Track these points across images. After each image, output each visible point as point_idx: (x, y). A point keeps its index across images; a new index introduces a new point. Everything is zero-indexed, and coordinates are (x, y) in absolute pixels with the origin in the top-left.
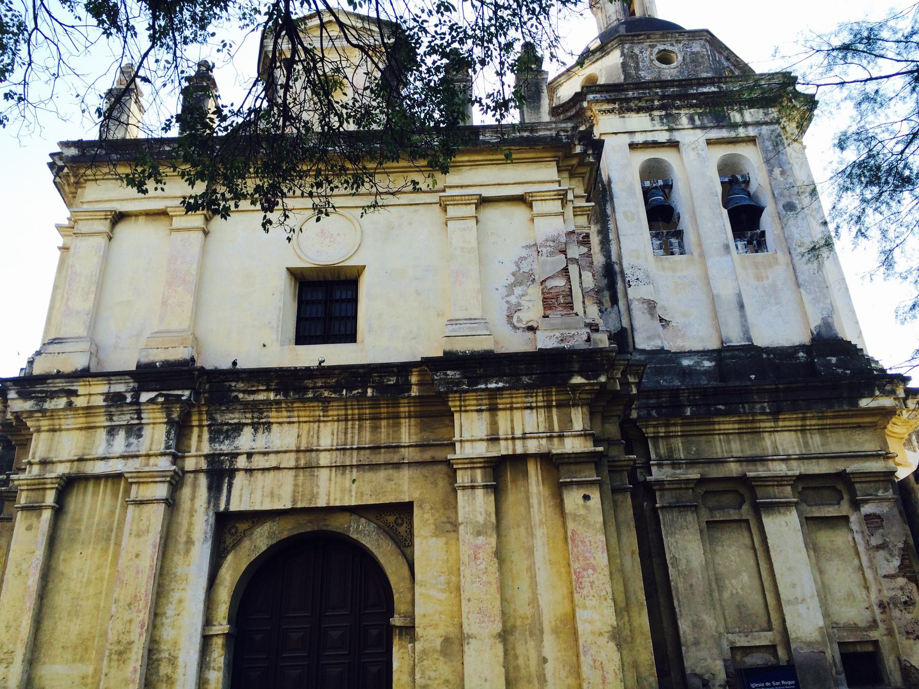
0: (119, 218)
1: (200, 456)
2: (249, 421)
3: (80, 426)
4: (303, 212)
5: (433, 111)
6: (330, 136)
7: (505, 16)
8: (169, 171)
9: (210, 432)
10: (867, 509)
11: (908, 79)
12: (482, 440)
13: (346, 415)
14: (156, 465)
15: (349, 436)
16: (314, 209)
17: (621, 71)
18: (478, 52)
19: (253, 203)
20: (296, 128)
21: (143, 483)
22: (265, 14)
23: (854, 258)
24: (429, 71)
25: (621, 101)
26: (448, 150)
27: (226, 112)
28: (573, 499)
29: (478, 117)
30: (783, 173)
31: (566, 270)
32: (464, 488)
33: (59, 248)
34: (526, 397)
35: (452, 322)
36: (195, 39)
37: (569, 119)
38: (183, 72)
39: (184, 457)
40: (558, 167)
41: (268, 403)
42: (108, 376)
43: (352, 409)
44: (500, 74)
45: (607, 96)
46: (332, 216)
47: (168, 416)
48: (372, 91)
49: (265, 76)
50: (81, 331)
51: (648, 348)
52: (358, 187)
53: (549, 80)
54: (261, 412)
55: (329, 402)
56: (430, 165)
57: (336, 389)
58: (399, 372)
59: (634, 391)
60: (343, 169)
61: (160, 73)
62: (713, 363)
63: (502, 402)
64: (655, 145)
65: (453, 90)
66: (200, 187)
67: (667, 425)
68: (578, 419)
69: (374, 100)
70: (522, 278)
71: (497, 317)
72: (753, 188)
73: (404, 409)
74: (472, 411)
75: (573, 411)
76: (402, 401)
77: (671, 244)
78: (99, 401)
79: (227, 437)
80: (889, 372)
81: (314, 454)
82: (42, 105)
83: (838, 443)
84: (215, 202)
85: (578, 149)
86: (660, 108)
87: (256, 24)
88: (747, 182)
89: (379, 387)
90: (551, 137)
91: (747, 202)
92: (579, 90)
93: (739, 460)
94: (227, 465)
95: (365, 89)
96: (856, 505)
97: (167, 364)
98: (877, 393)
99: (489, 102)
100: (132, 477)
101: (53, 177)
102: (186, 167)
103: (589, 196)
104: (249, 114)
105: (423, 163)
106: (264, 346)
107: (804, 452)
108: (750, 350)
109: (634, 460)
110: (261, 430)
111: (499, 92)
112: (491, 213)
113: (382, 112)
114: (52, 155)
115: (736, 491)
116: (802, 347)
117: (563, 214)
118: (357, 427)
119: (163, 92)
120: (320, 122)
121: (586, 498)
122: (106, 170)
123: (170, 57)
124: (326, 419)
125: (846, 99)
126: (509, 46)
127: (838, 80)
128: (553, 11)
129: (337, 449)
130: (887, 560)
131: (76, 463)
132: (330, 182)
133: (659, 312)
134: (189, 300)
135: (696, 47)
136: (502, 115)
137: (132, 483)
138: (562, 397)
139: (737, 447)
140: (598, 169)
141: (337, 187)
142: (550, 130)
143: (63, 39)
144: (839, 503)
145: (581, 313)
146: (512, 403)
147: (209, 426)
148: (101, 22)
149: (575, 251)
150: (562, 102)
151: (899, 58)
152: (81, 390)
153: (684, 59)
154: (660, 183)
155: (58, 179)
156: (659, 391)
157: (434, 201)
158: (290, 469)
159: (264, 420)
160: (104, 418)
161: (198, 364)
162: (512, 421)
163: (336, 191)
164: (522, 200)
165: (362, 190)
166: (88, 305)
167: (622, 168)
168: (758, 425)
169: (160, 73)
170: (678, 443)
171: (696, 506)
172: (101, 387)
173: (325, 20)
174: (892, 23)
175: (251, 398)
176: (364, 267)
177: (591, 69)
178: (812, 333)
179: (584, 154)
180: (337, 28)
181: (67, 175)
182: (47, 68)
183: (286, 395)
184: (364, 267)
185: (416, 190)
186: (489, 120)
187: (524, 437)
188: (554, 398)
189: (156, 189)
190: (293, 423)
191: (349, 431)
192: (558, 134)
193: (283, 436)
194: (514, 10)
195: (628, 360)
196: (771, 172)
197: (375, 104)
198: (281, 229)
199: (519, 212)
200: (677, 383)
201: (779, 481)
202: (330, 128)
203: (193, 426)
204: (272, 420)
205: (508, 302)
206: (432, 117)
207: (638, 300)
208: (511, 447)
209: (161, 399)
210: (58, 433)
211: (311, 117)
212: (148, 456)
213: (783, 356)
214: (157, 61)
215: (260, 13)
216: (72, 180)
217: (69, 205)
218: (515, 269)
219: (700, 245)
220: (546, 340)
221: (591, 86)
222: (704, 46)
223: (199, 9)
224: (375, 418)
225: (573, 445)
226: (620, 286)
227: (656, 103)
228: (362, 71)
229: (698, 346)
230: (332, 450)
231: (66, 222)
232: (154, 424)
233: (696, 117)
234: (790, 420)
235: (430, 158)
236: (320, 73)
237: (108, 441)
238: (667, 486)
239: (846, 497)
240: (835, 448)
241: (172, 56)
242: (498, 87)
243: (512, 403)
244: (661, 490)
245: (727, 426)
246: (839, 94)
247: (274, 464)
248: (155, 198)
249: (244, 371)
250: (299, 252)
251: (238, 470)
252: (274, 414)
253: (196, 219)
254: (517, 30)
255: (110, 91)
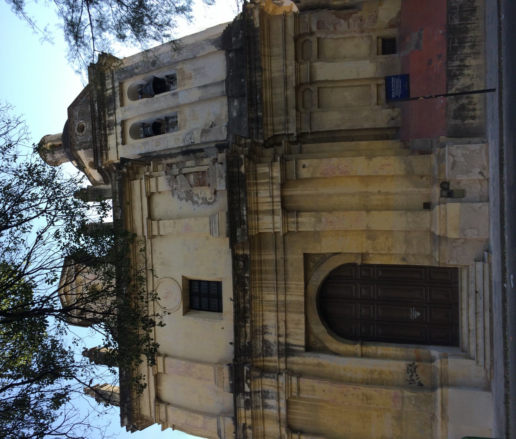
0: (158, 399)
1: (279, 361)
2: (261, 336)
3: (262, 423)
4: (155, 306)
5: (106, 241)
6: (118, 292)
7: (61, 205)
8: (135, 372)
9: (267, 356)
10: (314, 28)
11: (91, 6)
12: (273, 218)
13: (259, 287)
14: (282, 383)
15: (270, 285)
16: (154, 301)
17: (88, 150)
18: (78, 218)
19: (151, 331)
20: (114, 308)
21: (291, 390)
22: (60, 322)
23: (182, 29)
24: (86, 243)
25: (101, 150)
26: (125, 234)
27: (106, 343)
28: (305, 173)
29: (109, 219)
30: (137, 68)
31: (184, 174)
32: (297, 227)
33: (173, 430)
34: (251, 195)
35: (211, 233)
36: (72, 357)
37: (110, 175)
38: (87, 363)
39: (279, 369)
40: (133, 180)
41: (252, 326)
42: (236, 408)
43: (256, 284)
44: (88, 208)
45: (99, 156)
46: (157, 292)
47: (258, 377)
48: (97, 270)
49: (90, 323)
50: (215, 421)
51: (226, 133)
52: (144, 278)
53: (91, 185)
54: (256, 330)
55: (252, 296)
56: (132, 243)
57: (245, 291)
58: (237, 260)
59: (249, 140)
60: (134, 286)
61: (88, 374)
62: (236, 100)
63: (253, 208)
64: (123, 132)
65: (96, 231)
66: (144, 357)
67: (267, 125)
68: (263, 169)
69: (101, 269)
70: (189, 197)
71: (209, 210)
72: (144, 82)
73: (257, 258)
74: (258, 223)
75: (259, 172)
76: (252, 259)
77: (172, 122)
78: (249, 413)
79: (269, 347)
80: (241, 10)
81: (279, 303)
82: (103, 433)
83: (277, 38)
84: (151, 350)
85: (125, 170)
86: (105, 131)
87: (65, 327)
88: (141, 86)
89: (243, 269)
90: (119, 183)
91: (151, 85)
92: (96, 171)
93: (286, 89)
94: (283, 347)
95: (96, 274)
96: (312, 33)
97: (231, 378)
98: (252, 17)
99: (102, 213)
100: (288, 395)
101: (138, 431)
102: (133, 364)
103: (148, 164)
104: (108, 331)
105: (131, 246)
106: (223, 328)
107: (282, 57)
108: (228, 81)
109: (285, 142)
110: (266, 330)
111: (97, 208)
112: (157, 212)
113: (107, 266)
114: (127, 431)
115: (303, 92)
116: (227, 55)
117: (157, 177)
118: (265, 282)
119: (97, 373)
120: (112, 296)
121: (304, 166)
122: (135, 404)
123: (80, 369)
124: (261, 297)
125: (101, 36)
126: (75, 203)
127: (92, 41)
128: (59, 182)
129: (277, 291)
130: (341, 25)
131: (281, 424)
132: (141, 292)
133: (207, 128)
134: (198, 366)
135: (76, 114)
136: (108, 207)
137: (291, 395)
138: (252, 178)
139: (279, 90)
140: (134, 160)
141: (143, 289)
142: (115, 184)
143: (71, 421)
144: (311, 42)
145: (207, 167)
146: (254, 203)
147: (263, 356)
148: (63, 402)
149: (176, 171)
150: (102, 179)
151: (81, 10)
152: (243, 421)
153: (82, 119)
154: (141, 129)
155: (139, 428)
156: (249, 128)
157: (150, 242)
158: (286, 315)
159: (261, 329)
160: (258, 410)
161: (231, 362)
162: (264, 203)
163: (145, 290)
164: (150, 197)
165: (145, 276)
166: (201, 417)
167: (134, 148)
168: (267, 79)
169: (88, 374)
170: (276, 119)
171: (311, 113)
172: (242, 412)
173: (63, 293)
174: (65, 14)
175: (249, 335)
176: (183, 276)
177: (86, 164)
178: (219, 50)
179: (127, 167)
180: (67, 287)
181: (137, 423)
182: (85, 430)
183: (248, 317)
184: (183, 276)
185: (144, 250)
186: (110, 213)
187: (272, 197)
188: (252, 181)
189: (144, 379)
190: (262, 314)
191: (267, 285)
192: (117, 180)
193: (270, 319)
194: (58, 201)
195: (232, 143)
196: (136, 74)
197: (103, 269)
198: (164, 318)
199: (157, 199)
200: (245, 119)
201: (297, 71)
202: (114, 291)
203: (263, 365)
204: (261, 325)
205: (201, 204)
206: (110, 242)
207: (201, 138)
208: (277, 204)
209: (249, 381)
210: (266, 433)
211: (109, 301)
212: (278, 387)
213: (231, 65)
214: (82, 375)
215: (59, 324)
216: (140, 421)
217: (152, 424)
218: (184, 201)
219: (172, 108)
220: (221, 185)
221: (94, 165)
222: (76, 110)
223: (57, 355)
224: (261, 272)
225: (277, 173)
226: (193, 148)
227: (103, 132)
228: (87, 276)
229: (226, 108)
230: (277, 294)
231: (160, 425)
232: (262, 385)
233: (110, 112)
234: (265, 62)
235: (129, 242)
236: (88, 296)
237: (270, 408)
238: (299, 126)
239: (308, 37)
240: (280, 42)
241: (80, 368)
242: (94, 209)
243: (254, 203)
244: (301, 130)
245: (268, 94)
246: (98, 40)
247: (283, 323)
248: (148, 380)
249: (235, 339)
250: (176, 309)
251: (286, 341)
252: (258, 324)
253: (159, 360)
254: (68, 200)
255: (97, 400)
